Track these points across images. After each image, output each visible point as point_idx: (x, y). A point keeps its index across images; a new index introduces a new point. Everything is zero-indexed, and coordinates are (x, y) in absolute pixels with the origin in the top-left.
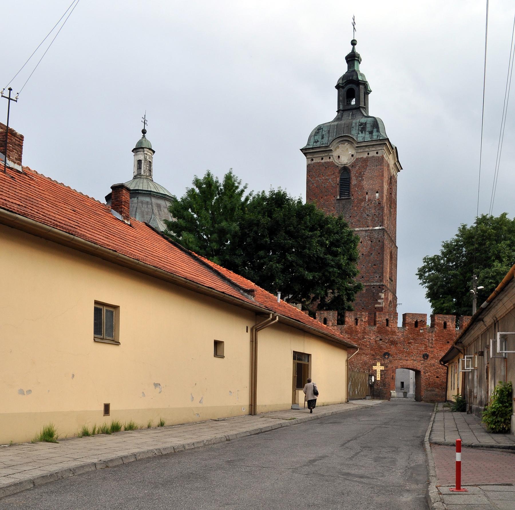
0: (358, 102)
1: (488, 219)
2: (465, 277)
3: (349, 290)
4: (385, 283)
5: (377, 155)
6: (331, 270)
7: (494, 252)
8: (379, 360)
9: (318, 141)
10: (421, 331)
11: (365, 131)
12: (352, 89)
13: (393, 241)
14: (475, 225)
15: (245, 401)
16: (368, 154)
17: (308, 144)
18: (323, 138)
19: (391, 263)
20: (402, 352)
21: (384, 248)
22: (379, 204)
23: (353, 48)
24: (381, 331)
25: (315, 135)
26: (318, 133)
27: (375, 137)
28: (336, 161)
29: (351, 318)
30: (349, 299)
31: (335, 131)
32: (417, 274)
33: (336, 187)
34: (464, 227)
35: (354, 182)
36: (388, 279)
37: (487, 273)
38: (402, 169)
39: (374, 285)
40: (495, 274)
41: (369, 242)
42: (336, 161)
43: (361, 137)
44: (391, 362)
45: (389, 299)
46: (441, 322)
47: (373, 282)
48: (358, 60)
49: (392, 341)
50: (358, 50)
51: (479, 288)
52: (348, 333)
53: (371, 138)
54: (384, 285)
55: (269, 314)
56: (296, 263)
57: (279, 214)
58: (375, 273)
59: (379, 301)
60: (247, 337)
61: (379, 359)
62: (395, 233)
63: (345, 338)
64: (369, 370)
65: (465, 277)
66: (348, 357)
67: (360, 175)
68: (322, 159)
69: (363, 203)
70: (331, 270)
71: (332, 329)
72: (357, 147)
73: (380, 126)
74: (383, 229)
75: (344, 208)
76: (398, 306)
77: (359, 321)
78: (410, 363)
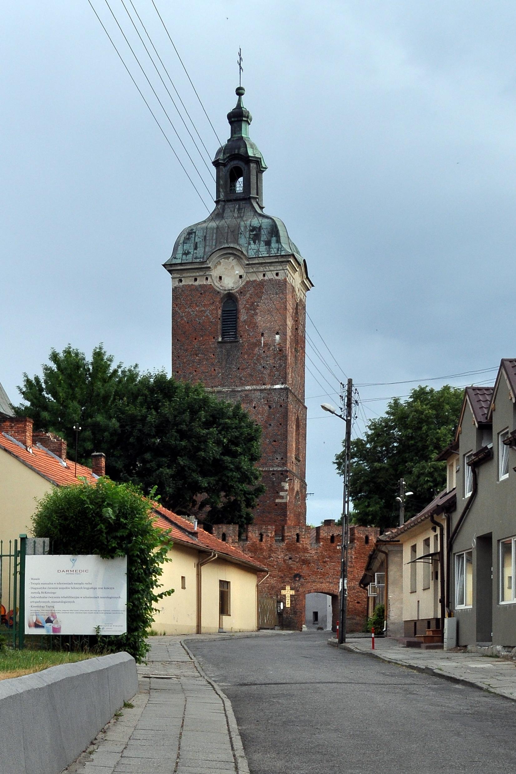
0: (247, 185)
1: (427, 393)
2: (396, 470)
3: (249, 494)
4: (289, 467)
5: (277, 278)
6: (230, 474)
7: (432, 439)
8: (289, 583)
9: (189, 253)
10: (338, 548)
11: (259, 242)
12: (237, 166)
13: (300, 402)
14: (411, 400)
15: (194, 623)
16: (264, 275)
17: (174, 257)
18: (196, 248)
19: (298, 434)
20: (316, 573)
21: (288, 412)
22: (280, 350)
23: (240, 100)
24: (291, 548)
25: (184, 243)
26: (188, 239)
27: (273, 252)
28: (217, 284)
29: (255, 533)
30: (248, 505)
31: (214, 237)
32: (334, 463)
33: (216, 325)
34: (396, 401)
35: (243, 317)
36: (294, 460)
37: (424, 467)
38: (313, 286)
39: (274, 471)
40: (432, 470)
41: (267, 408)
42: (216, 284)
43: (252, 249)
44: (302, 585)
45: (296, 489)
46: (361, 536)
47: (273, 466)
48: (247, 121)
49: (303, 560)
50: (246, 105)
51: (407, 494)
52: (251, 552)
53: (269, 252)
54: (290, 471)
55: (211, 553)
56: (189, 468)
57: (167, 409)
58: (275, 452)
59: (282, 494)
60: (194, 570)
61: (288, 581)
62: (304, 386)
63: (247, 557)
64: (277, 596)
65: (396, 470)
66: (259, 581)
67: (253, 307)
68: (196, 280)
69: (257, 349)
70: (230, 474)
71: (232, 547)
72: (247, 264)
73: (281, 233)
74: (286, 389)
75: (228, 355)
76: (308, 497)
77: (264, 536)
78: (325, 586)
